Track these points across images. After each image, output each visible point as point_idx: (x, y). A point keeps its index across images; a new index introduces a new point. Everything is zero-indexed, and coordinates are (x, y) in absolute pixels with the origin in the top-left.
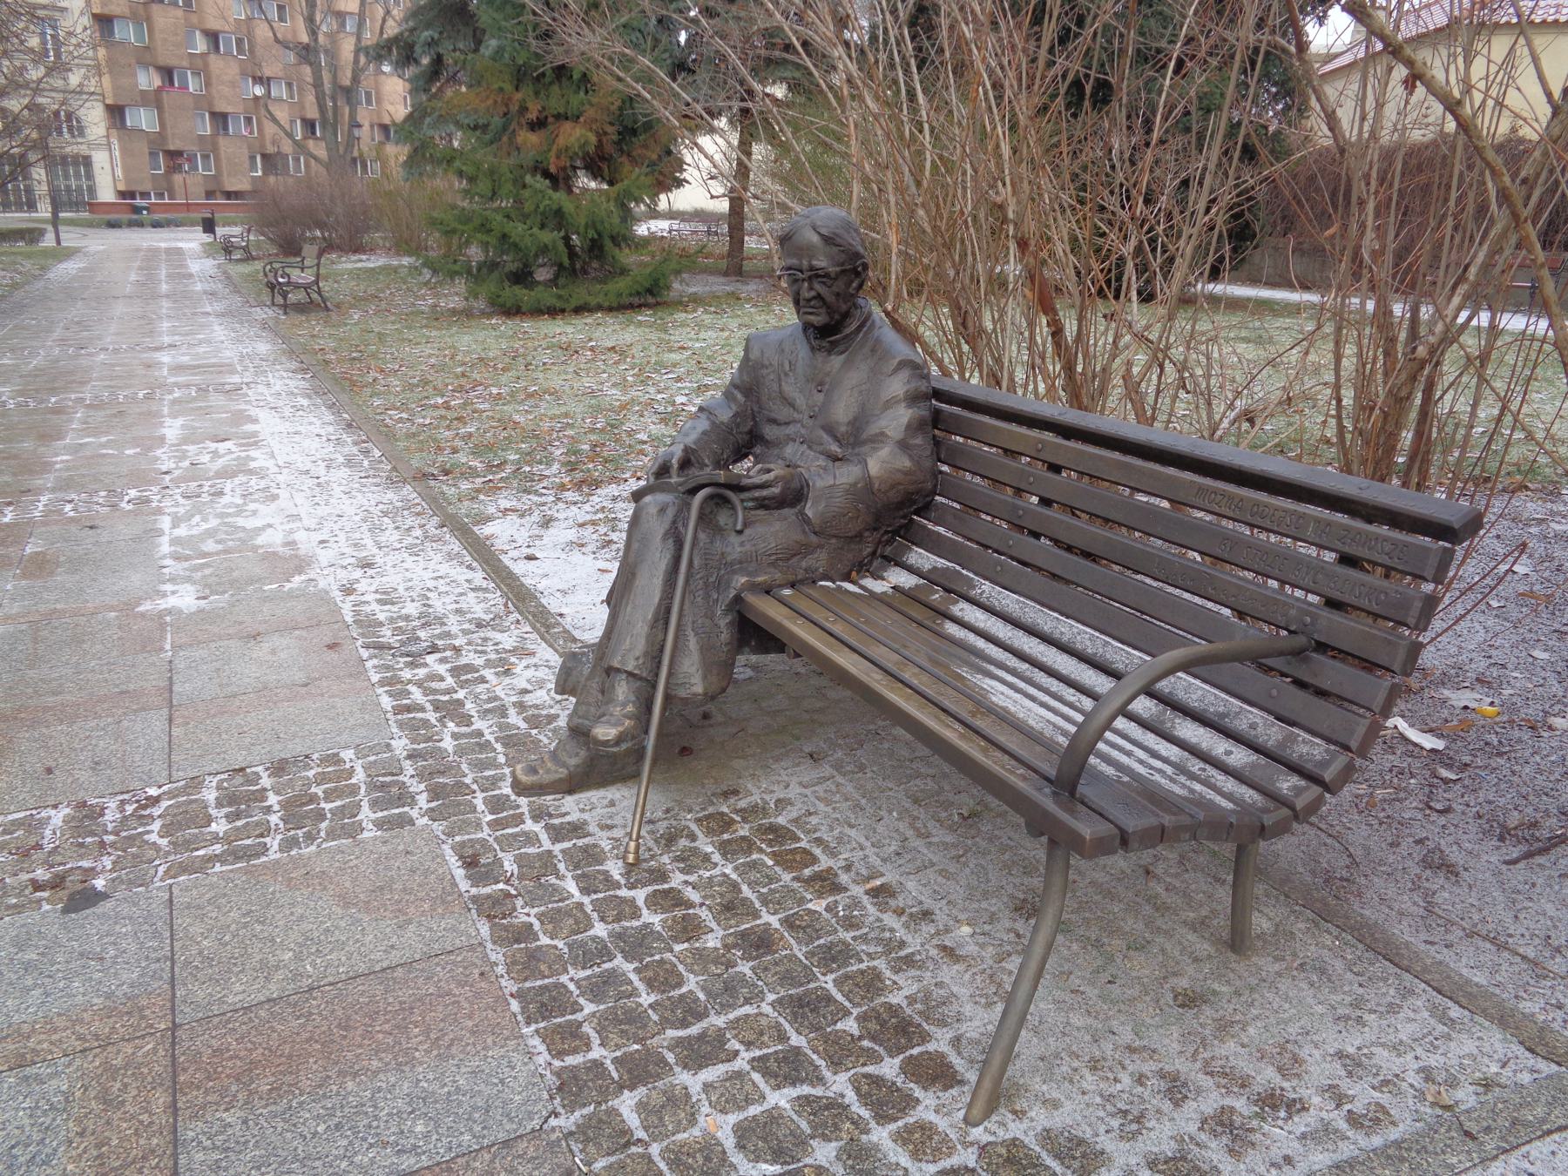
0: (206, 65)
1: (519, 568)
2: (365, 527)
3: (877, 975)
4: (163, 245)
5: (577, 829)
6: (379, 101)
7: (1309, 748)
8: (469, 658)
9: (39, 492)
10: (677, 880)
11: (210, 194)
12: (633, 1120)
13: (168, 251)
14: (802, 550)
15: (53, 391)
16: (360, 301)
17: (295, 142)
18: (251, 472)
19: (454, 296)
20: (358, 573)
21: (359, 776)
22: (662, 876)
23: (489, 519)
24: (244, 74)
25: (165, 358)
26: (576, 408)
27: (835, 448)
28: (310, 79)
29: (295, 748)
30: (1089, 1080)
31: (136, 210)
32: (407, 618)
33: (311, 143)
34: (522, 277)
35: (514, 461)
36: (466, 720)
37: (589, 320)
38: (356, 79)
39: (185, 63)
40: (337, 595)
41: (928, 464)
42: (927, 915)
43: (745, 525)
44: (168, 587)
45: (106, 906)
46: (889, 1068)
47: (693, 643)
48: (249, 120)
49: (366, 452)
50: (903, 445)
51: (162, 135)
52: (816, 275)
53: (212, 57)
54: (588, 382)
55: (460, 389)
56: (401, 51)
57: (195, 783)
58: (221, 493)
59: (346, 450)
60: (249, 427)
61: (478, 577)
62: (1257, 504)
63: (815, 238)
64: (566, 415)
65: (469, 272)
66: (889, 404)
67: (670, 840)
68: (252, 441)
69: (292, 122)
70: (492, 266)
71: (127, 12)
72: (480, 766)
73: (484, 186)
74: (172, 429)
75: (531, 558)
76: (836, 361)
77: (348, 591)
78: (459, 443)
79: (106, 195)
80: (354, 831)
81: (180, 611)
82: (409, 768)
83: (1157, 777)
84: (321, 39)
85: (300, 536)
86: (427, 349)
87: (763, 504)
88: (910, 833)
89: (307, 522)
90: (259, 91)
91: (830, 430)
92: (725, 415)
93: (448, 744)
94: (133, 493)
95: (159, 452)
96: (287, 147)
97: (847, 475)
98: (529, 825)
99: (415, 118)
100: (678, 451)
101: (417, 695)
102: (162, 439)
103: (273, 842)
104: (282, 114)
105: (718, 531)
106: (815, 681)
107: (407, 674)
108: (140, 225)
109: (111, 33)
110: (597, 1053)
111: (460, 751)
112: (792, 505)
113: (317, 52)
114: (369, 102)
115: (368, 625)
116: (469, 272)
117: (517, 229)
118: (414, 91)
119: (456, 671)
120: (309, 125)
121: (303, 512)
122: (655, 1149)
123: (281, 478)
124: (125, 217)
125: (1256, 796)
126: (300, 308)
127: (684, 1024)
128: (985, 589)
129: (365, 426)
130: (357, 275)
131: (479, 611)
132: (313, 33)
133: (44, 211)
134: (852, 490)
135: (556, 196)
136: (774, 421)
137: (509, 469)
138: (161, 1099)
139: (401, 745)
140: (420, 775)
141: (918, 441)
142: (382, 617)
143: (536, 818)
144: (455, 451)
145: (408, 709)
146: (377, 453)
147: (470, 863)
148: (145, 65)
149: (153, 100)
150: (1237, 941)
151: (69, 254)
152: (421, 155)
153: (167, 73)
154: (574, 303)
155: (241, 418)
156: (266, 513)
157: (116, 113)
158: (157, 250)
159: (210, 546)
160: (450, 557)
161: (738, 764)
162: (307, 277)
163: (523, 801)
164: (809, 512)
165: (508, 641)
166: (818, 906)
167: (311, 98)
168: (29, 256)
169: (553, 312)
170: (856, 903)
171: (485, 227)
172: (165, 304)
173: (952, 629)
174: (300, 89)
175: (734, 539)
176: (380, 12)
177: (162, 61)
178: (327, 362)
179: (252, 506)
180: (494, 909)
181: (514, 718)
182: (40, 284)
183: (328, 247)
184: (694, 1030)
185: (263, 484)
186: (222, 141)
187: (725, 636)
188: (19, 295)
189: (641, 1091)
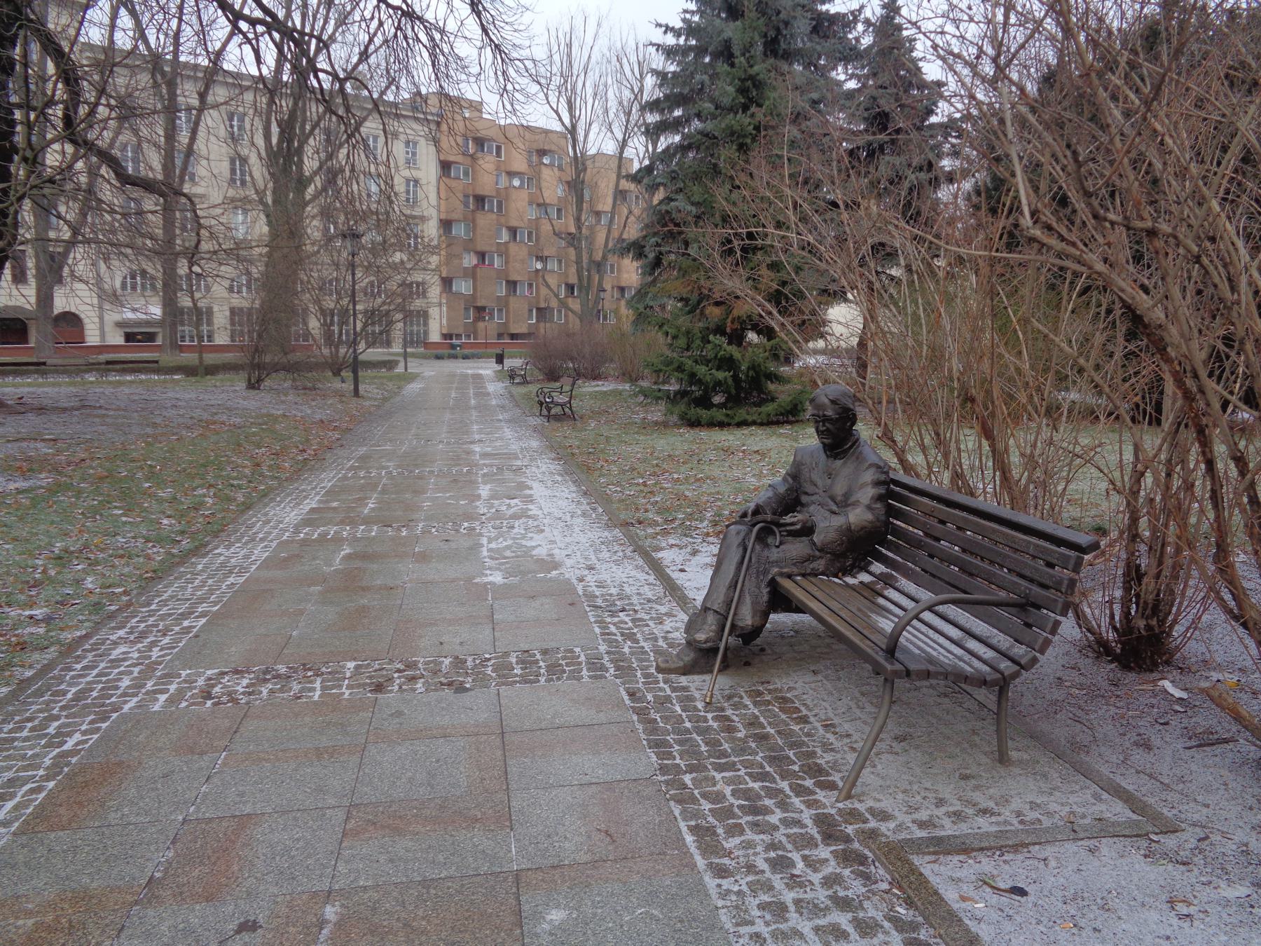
0: (507, 249)
1: (675, 575)
2: (591, 549)
3: (815, 753)
4: (470, 372)
5: (685, 689)
6: (619, 271)
7: (1019, 650)
8: (641, 615)
9: (418, 521)
10: (729, 712)
11: (500, 336)
12: (689, 783)
13: (473, 375)
14: (810, 559)
15: (416, 466)
16: (596, 414)
17: (559, 300)
18: (529, 517)
19: (657, 413)
20: (586, 572)
21: (582, 658)
22: (723, 710)
23: (662, 549)
24: (530, 254)
25: (477, 448)
26: (726, 489)
27: (834, 508)
28: (573, 258)
29: (553, 645)
30: (900, 796)
31: (453, 347)
32: (611, 595)
33: (570, 300)
34: (704, 402)
35: (679, 518)
36: (637, 642)
37: (745, 432)
38: (604, 257)
39: (494, 249)
40: (575, 582)
41: (883, 518)
42: (848, 736)
43: (781, 543)
44: (488, 572)
45: (469, 693)
46: (809, 783)
47: (748, 600)
48: (530, 285)
49: (594, 509)
50: (869, 508)
51: (474, 296)
52: (826, 419)
53: (512, 245)
54: (737, 473)
55: (654, 474)
56: (637, 249)
57: (507, 654)
58: (513, 527)
59: (583, 507)
60: (528, 492)
61: (652, 578)
62: (1013, 537)
63: (826, 401)
64: (718, 493)
65: (668, 397)
66: (863, 486)
67: (729, 697)
68: (530, 500)
69: (559, 286)
70: (682, 394)
71: (461, 217)
72: (641, 660)
73: (682, 342)
74: (484, 491)
75: (682, 570)
76: (839, 463)
77: (581, 580)
78: (649, 506)
79: (435, 337)
80: (579, 679)
81: (494, 584)
82: (606, 658)
83: (942, 658)
84: (584, 231)
85: (556, 551)
86: (636, 447)
87: (790, 533)
88: (854, 706)
89: (559, 545)
90: (539, 266)
91: (833, 499)
92: (782, 490)
93: (626, 650)
94: (466, 524)
95: (478, 503)
96: (554, 303)
97: (838, 521)
98: (662, 685)
99: (641, 293)
100: (752, 506)
101: (613, 629)
102: (479, 496)
103: (542, 679)
104: (552, 281)
105: (767, 546)
106: (828, 640)
107: (609, 620)
108: (455, 357)
109: (450, 232)
110: (678, 761)
111: (632, 653)
112: (807, 536)
113: (580, 240)
114: (612, 272)
115: (591, 597)
116: (668, 397)
117: (701, 370)
118: (643, 274)
119: (633, 621)
120: (570, 288)
121: (558, 539)
122: (696, 792)
123: (545, 521)
124: (446, 352)
125: (988, 669)
126: (557, 418)
127: (719, 758)
128: (904, 583)
129: (594, 494)
130: (594, 396)
131: (650, 595)
132: (579, 228)
133: (397, 348)
134: (839, 530)
135: (729, 348)
136: (806, 493)
137: (677, 523)
138: (499, 753)
139: (603, 648)
140: (611, 661)
141: (878, 505)
142: (597, 593)
143: (665, 683)
144: (646, 511)
145: (608, 634)
146: (601, 510)
147: (632, 695)
148: (467, 250)
149: (471, 273)
150: (1002, 758)
151: (412, 378)
152: (641, 318)
153: (482, 255)
154: (737, 419)
155: (522, 486)
156: (537, 539)
157: (447, 282)
158: (466, 375)
159: (508, 553)
160: (637, 567)
161: (772, 671)
162: (563, 399)
163: (660, 676)
164: (815, 539)
165: (663, 609)
166: (796, 728)
167: (573, 269)
168: (390, 379)
169: (722, 425)
170: (815, 728)
171: (680, 369)
172: (474, 413)
173: (881, 601)
174: (567, 266)
175: (775, 550)
176: (626, 211)
177: (479, 248)
178: (573, 454)
179: (530, 535)
180: (641, 712)
181: (661, 643)
182: (398, 399)
183: (578, 375)
184: (723, 761)
185: (536, 523)
186: (512, 299)
187: (765, 598)
188: (387, 405)
189: (694, 775)
